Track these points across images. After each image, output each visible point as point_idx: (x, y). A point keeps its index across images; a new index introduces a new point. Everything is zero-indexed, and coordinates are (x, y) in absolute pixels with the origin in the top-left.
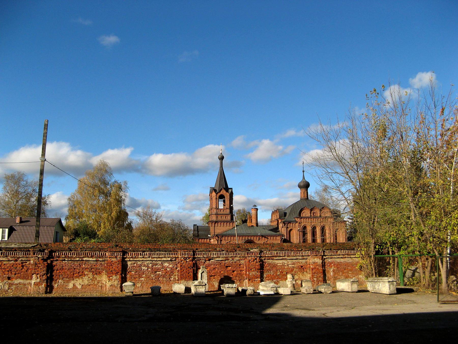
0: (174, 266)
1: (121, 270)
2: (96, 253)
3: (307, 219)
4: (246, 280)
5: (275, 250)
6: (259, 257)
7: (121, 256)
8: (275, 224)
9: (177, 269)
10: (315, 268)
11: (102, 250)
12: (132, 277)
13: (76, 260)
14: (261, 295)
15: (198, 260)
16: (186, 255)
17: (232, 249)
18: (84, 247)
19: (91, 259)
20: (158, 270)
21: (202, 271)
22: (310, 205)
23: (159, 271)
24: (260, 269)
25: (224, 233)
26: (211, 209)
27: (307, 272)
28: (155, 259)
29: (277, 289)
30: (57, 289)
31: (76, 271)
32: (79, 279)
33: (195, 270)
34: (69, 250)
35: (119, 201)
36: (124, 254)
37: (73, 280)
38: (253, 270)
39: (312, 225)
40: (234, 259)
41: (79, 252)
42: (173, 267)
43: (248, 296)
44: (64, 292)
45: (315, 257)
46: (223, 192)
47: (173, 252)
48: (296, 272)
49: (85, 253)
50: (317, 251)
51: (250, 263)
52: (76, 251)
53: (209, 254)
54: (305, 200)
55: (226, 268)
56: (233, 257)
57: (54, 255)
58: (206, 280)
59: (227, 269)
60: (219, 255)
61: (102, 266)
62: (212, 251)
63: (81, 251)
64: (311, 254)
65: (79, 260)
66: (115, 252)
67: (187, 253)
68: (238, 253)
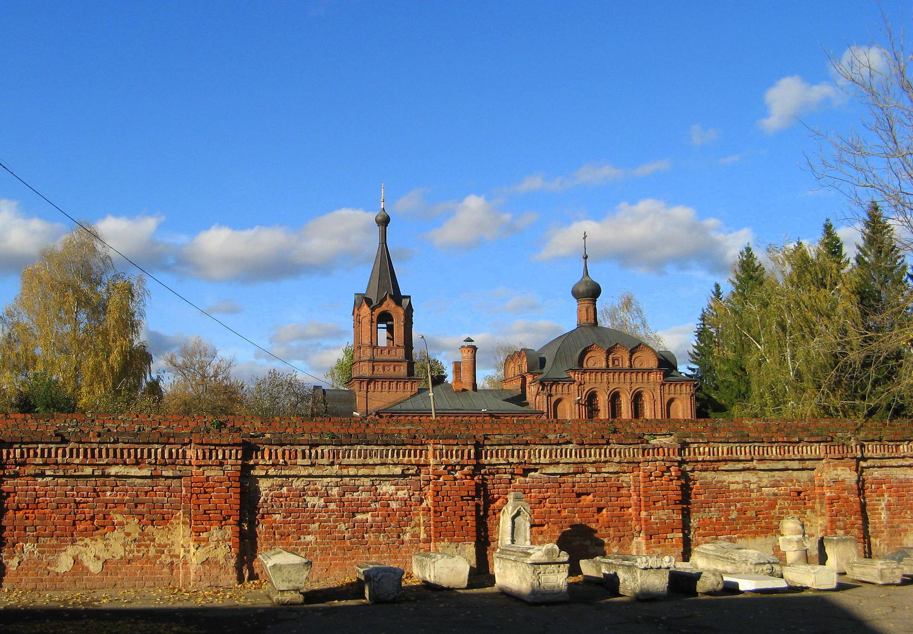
0: (413, 494)
1: (238, 507)
2: (153, 451)
3: (599, 374)
4: (640, 538)
5: (723, 440)
6: (676, 464)
7: (240, 462)
8: (515, 386)
9: (421, 504)
10: (839, 498)
11: (172, 440)
12: (274, 534)
13: (83, 474)
14: (742, 592)
15: (490, 474)
16: (452, 457)
17: (594, 438)
18: (109, 430)
19: (134, 471)
20: (362, 507)
21: (516, 511)
22: (603, 341)
23: (364, 512)
24: (681, 502)
25: (394, 408)
26: (359, 346)
27: (813, 509)
28: (352, 471)
29: (773, 568)
30: (18, 574)
31: (84, 513)
32: (92, 540)
33: (482, 507)
34: (59, 439)
35: (129, 324)
36: (247, 456)
37: (73, 542)
38: (660, 504)
39: (611, 389)
40: (603, 470)
41: (94, 446)
42: (410, 497)
43: (700, 597)
44: (40, 586)
45: (836, 462)
46: (389, 305)
47: (409, 447)
48: (785, 511)
49: (115, 450)
50: (843, 445)
51: (651, 481)
52: (84, 443)
53: (527, 452)
54: (589, 327)
55: (577, 500)
56: (600, 462)
57: (5, 457)
58: (526, 540)
59: (579, 501)
60: (556, 456)
61: (171, 496)
62: (534, 444)
63: (99, 443)
64: (827, 453)
65: (93, 476)
66: (217, 448)
67: (457, 451)
68: (613, 450)
